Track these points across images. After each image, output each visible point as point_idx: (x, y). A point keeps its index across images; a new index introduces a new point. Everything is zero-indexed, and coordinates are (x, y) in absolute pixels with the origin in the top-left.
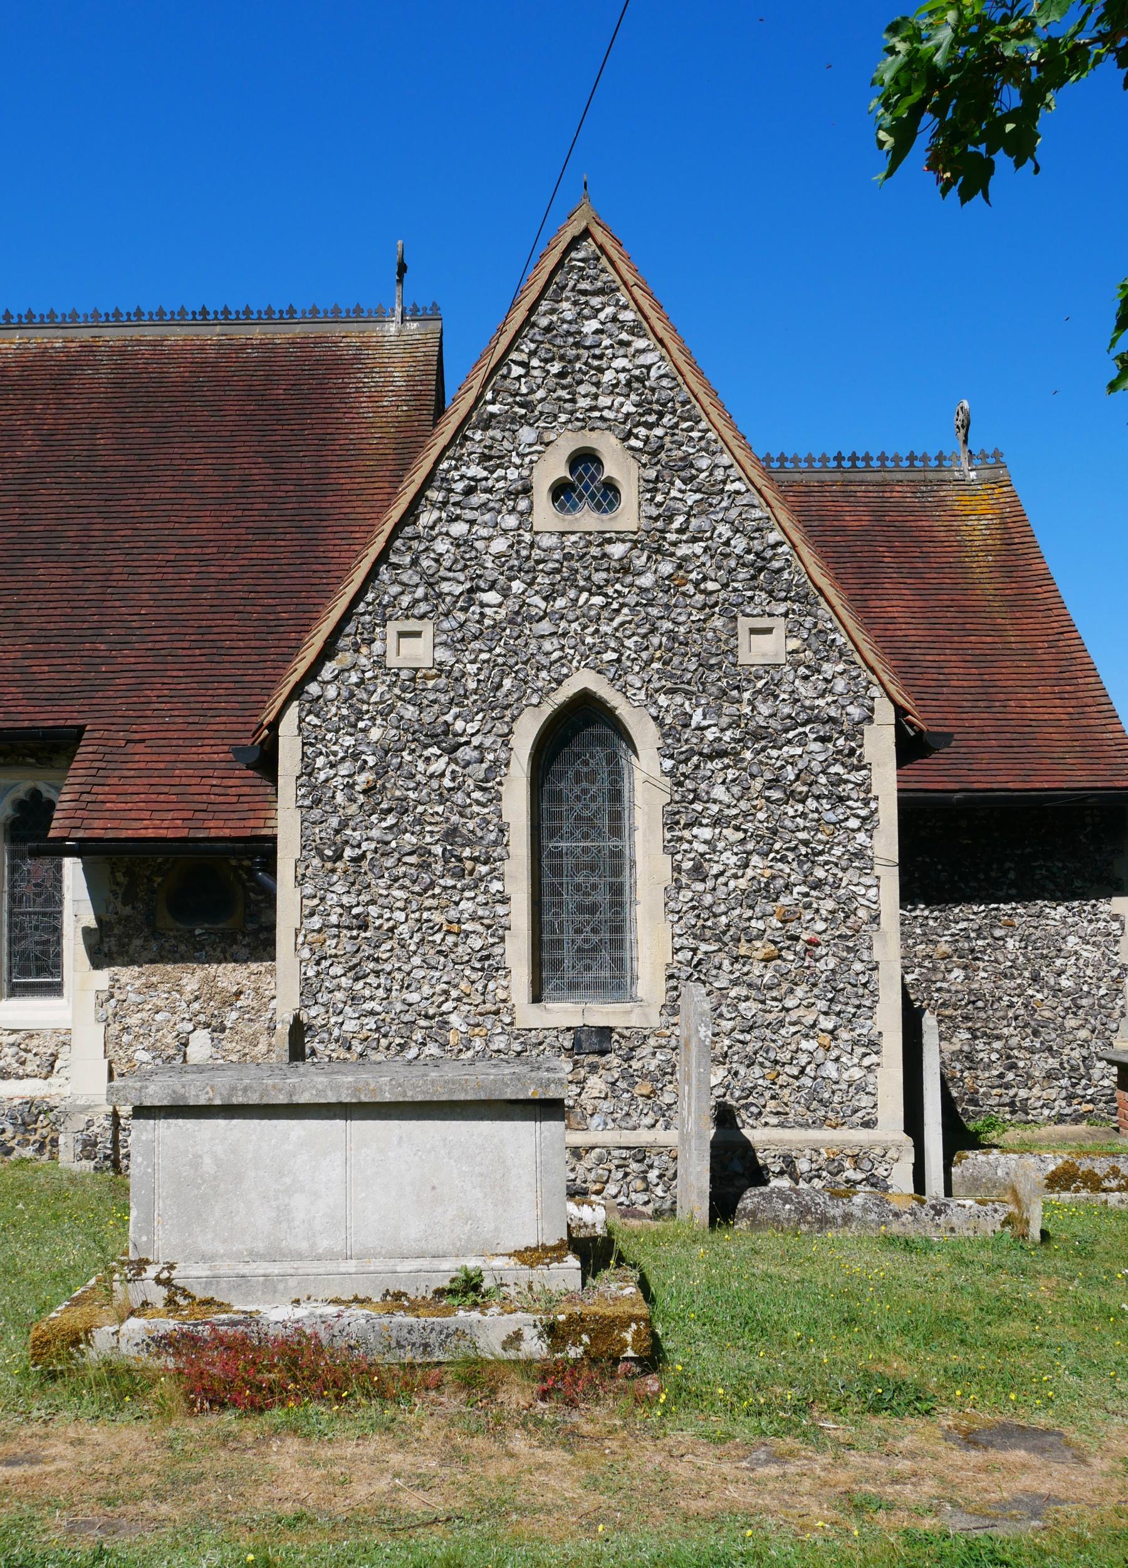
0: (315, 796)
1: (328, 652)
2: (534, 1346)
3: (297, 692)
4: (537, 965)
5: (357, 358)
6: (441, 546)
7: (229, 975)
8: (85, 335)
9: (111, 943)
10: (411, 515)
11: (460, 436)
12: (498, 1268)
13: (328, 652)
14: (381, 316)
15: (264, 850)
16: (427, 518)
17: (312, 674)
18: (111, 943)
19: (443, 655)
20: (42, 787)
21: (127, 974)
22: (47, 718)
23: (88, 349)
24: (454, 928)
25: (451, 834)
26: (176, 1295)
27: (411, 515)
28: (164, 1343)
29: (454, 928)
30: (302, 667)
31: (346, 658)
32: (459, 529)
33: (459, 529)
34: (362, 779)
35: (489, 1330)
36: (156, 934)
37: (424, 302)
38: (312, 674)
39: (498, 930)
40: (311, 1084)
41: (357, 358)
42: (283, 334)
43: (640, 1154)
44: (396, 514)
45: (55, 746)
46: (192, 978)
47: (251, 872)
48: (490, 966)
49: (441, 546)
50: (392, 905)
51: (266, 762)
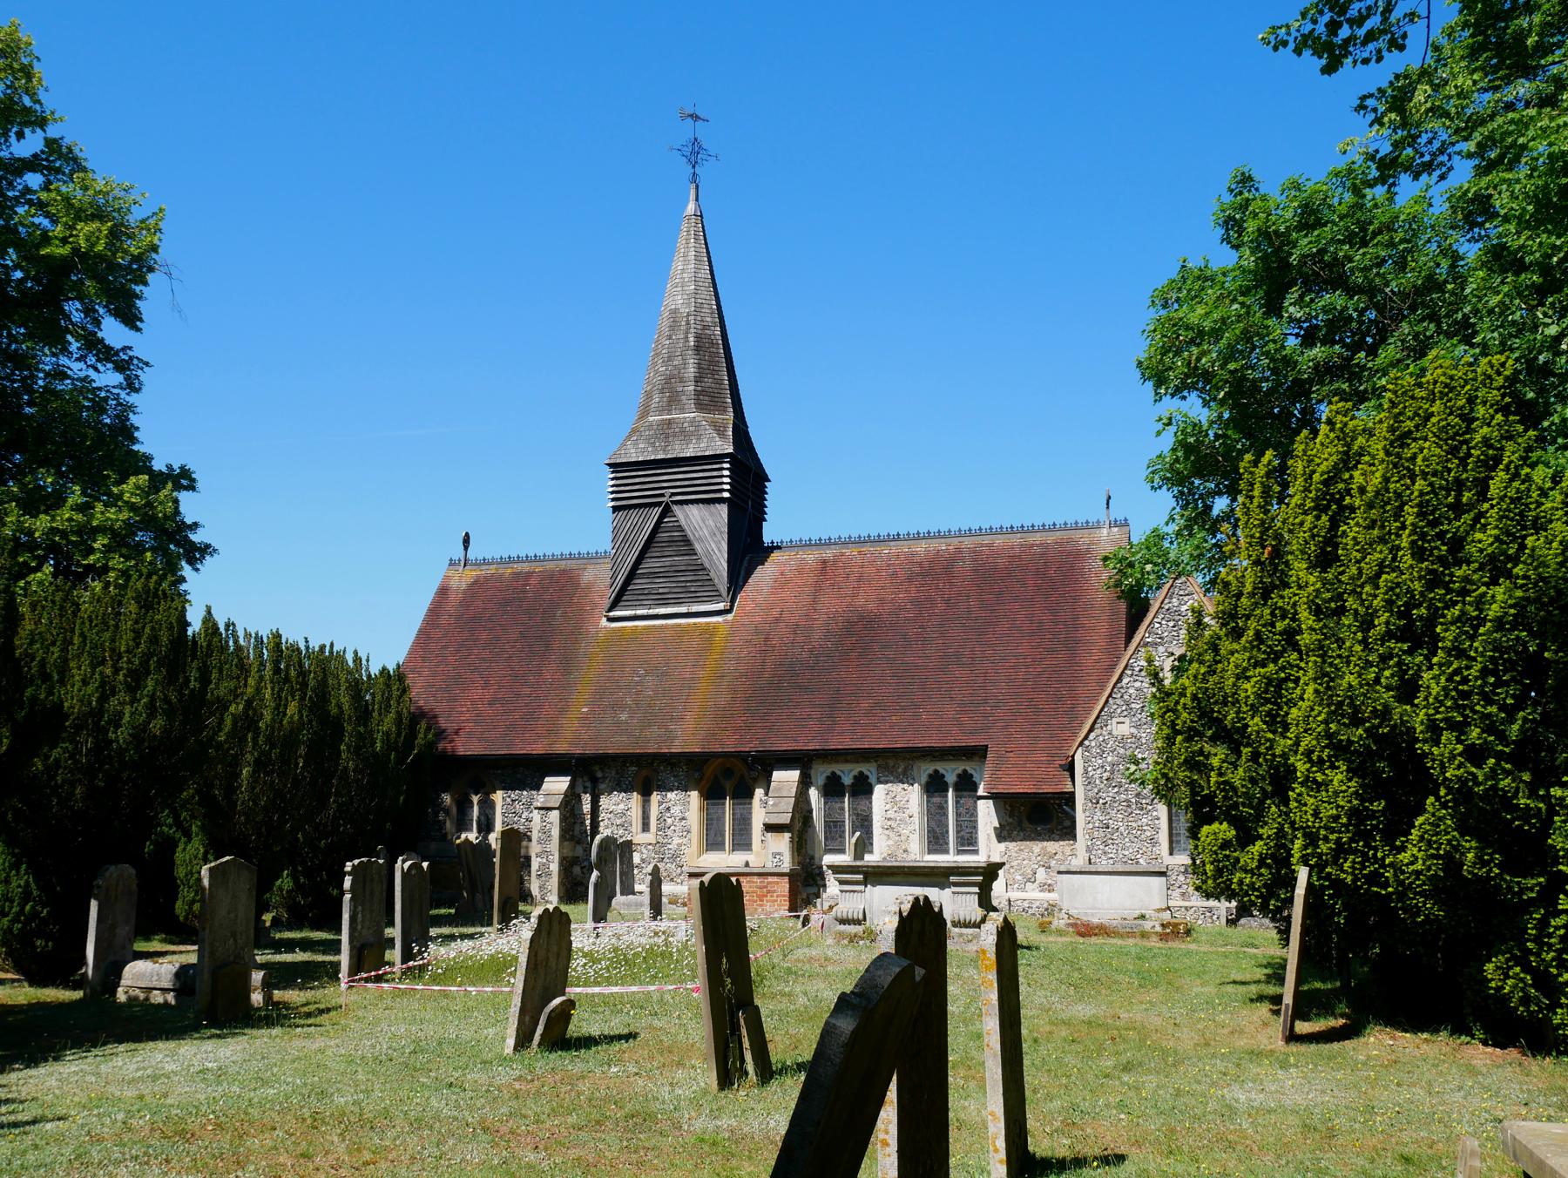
0: (1089, 782)
1: (1091, 730)
2: (1158, 929)
3: (1081, 744)
4: (1171, 842)
5: (1088, 551)
6: (1131, 691)
7: (1052, 846)
8: (955, 541)
9: (1005, 833)
10: (1120, 679)
11: (1136, 650)
12: (1148, 913)
13: (1091, 730)
14: (1098, 526)
15: (1070, 798)
16: (1125, 680)
17: (1086, 738)
18: (1005, 833)
19: (1133, 730)
20: (970, 771)
21: (1011, 845)
22: (972, 741)
23: (959, 550)
24: (1140, 828)
25: (1138, 795)
26: (1070, 916)
27: (1120, 679)
28: (1069, 925)
29: (1140, 828)
30: (1082, 735)
31: (1097, 732)
32: (1137, 684)
33: (1137, 684)
34: (1106, 775)
35: (1147, 925)
36: (1022, 830)
37: (1120, 517)
38: (1086, 738)
39: (1157, 830)
40: (1093, 868)
41: (1088, 551)
42: (1051, 538)
43: (1210, 910)
44: (1114, 680)
45: (977, 753)
46: (1037, 847)
47: (1060, 806)
48: (1153, 842)
49: (1131, 691)
50: (1117, 820)
51: (1070, 768)
